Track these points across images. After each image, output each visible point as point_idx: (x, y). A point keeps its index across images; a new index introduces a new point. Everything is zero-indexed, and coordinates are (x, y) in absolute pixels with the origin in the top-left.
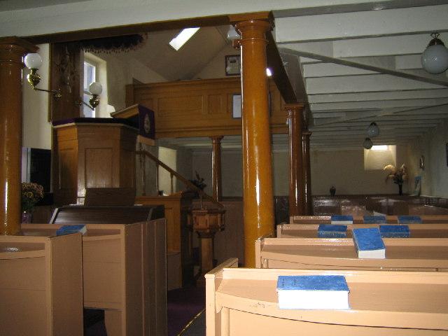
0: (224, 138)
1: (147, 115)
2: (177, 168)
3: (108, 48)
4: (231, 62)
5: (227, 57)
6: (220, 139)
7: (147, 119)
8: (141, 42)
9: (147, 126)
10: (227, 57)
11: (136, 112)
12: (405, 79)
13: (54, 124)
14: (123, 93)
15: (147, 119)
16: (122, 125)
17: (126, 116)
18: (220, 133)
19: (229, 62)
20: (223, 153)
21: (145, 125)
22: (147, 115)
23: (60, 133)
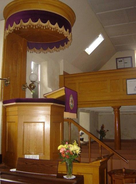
0: (122, 107)
1: (71, 96)
2: (90, 128)
3: (45, 49)
4: (119, 61)
5: (117, 59)
6: (119, 108)
7: (71, 98)
8: (67, 44)
9: (71, 104)
10: (117, 59)
11: (63, 93)
12: (8, 3)
13: (4, 102)
14: (58, 80)
15: (71, 98)
16: (52, 104)
17: (55, 97)
18: (119, 105)
19: (118, 61)
20: (120, 113)
21: (70, 103)
22: (71, 96)
23: (9, 110)
